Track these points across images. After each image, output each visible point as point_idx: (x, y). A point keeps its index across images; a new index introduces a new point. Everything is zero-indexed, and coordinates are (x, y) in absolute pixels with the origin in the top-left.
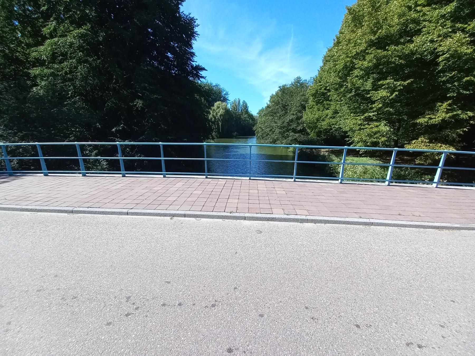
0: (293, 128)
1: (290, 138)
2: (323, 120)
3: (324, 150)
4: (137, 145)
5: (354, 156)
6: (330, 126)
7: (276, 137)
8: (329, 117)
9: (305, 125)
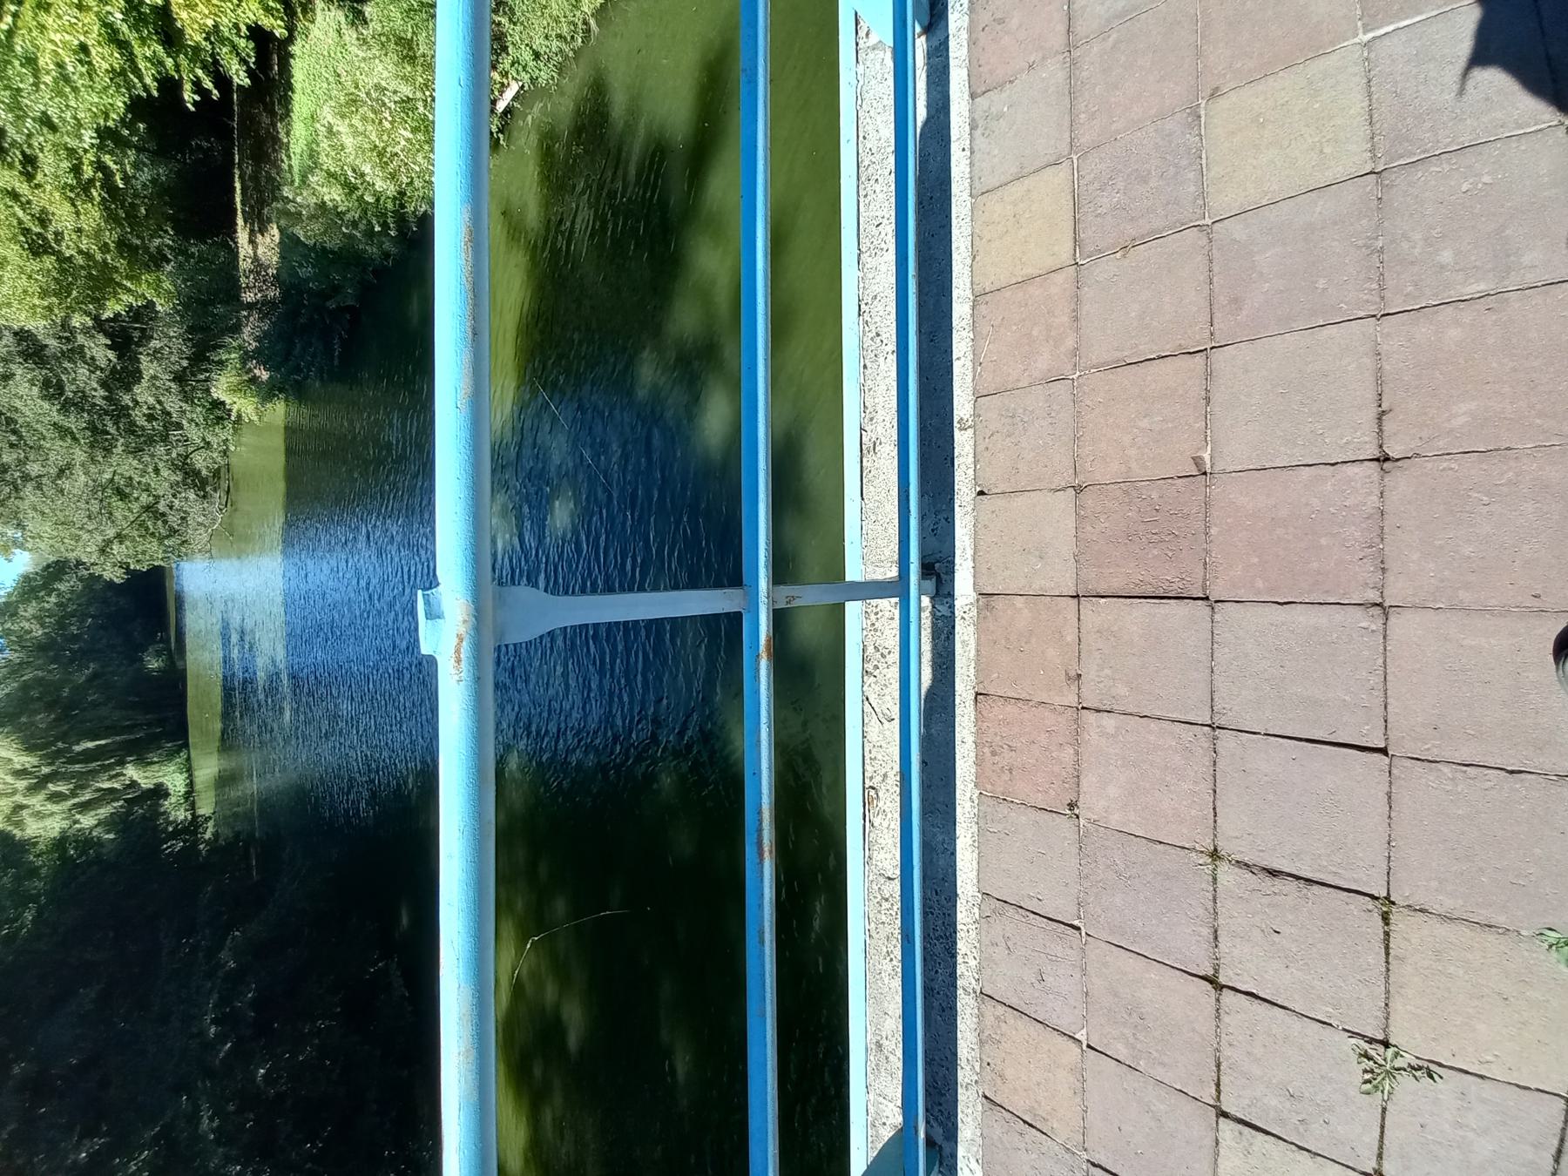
0: (104, 384)
1: (173, 404)
2: (43, 220)
3: (257, 248)
4: (923, 517)
5: (288, 113)
6: (86, 187)
7: (165, 473)
8: (23, 188)
9: (77, 321)
